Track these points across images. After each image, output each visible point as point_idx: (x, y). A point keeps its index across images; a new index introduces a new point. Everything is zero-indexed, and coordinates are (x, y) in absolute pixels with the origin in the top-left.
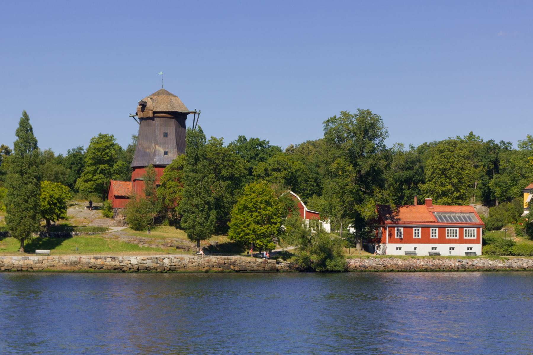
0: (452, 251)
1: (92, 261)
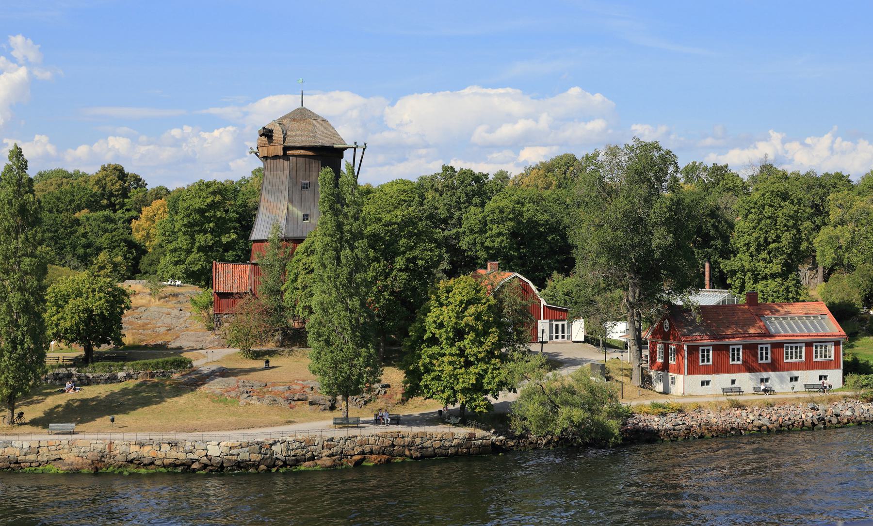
0: (794, 383)
1: (134, 448)
